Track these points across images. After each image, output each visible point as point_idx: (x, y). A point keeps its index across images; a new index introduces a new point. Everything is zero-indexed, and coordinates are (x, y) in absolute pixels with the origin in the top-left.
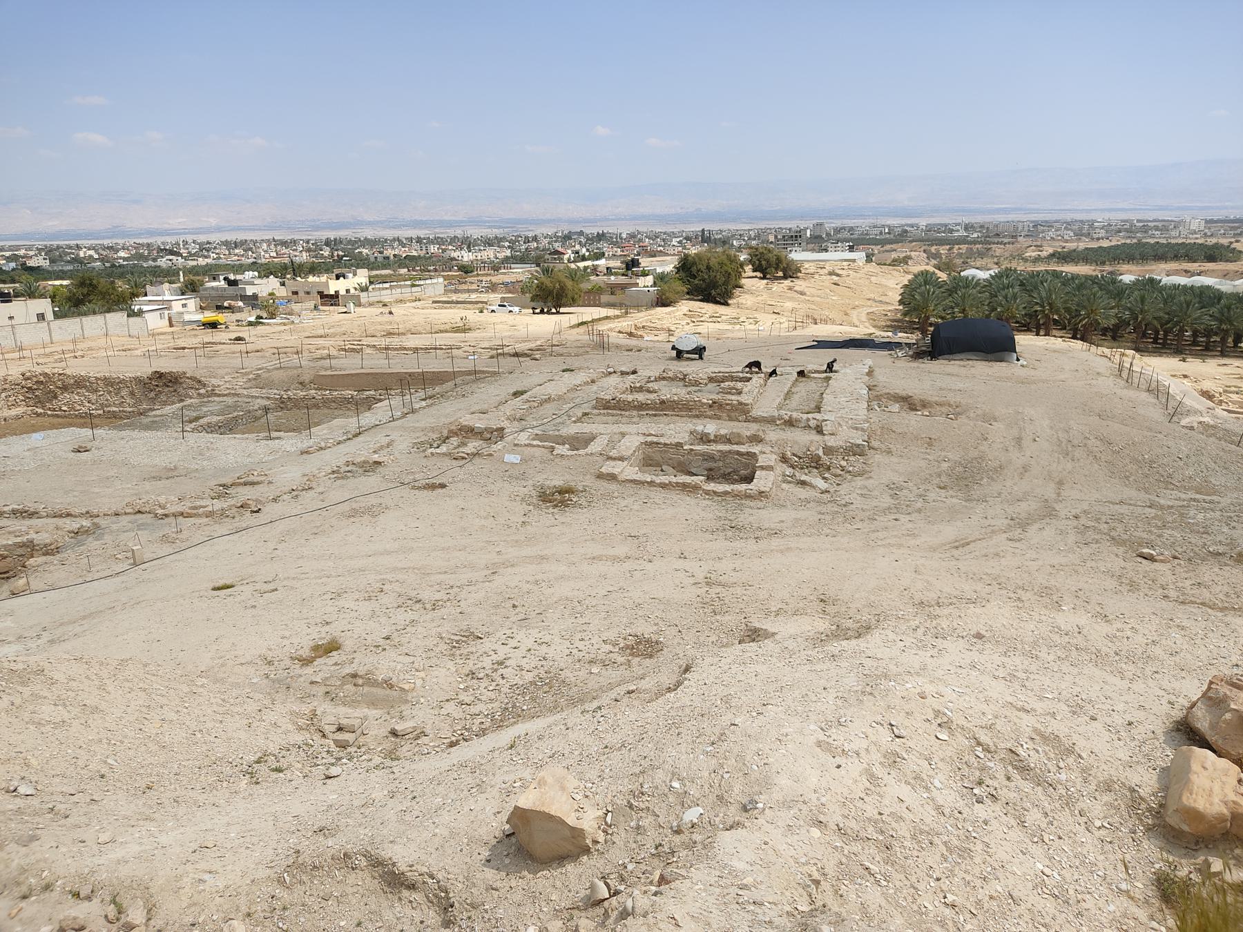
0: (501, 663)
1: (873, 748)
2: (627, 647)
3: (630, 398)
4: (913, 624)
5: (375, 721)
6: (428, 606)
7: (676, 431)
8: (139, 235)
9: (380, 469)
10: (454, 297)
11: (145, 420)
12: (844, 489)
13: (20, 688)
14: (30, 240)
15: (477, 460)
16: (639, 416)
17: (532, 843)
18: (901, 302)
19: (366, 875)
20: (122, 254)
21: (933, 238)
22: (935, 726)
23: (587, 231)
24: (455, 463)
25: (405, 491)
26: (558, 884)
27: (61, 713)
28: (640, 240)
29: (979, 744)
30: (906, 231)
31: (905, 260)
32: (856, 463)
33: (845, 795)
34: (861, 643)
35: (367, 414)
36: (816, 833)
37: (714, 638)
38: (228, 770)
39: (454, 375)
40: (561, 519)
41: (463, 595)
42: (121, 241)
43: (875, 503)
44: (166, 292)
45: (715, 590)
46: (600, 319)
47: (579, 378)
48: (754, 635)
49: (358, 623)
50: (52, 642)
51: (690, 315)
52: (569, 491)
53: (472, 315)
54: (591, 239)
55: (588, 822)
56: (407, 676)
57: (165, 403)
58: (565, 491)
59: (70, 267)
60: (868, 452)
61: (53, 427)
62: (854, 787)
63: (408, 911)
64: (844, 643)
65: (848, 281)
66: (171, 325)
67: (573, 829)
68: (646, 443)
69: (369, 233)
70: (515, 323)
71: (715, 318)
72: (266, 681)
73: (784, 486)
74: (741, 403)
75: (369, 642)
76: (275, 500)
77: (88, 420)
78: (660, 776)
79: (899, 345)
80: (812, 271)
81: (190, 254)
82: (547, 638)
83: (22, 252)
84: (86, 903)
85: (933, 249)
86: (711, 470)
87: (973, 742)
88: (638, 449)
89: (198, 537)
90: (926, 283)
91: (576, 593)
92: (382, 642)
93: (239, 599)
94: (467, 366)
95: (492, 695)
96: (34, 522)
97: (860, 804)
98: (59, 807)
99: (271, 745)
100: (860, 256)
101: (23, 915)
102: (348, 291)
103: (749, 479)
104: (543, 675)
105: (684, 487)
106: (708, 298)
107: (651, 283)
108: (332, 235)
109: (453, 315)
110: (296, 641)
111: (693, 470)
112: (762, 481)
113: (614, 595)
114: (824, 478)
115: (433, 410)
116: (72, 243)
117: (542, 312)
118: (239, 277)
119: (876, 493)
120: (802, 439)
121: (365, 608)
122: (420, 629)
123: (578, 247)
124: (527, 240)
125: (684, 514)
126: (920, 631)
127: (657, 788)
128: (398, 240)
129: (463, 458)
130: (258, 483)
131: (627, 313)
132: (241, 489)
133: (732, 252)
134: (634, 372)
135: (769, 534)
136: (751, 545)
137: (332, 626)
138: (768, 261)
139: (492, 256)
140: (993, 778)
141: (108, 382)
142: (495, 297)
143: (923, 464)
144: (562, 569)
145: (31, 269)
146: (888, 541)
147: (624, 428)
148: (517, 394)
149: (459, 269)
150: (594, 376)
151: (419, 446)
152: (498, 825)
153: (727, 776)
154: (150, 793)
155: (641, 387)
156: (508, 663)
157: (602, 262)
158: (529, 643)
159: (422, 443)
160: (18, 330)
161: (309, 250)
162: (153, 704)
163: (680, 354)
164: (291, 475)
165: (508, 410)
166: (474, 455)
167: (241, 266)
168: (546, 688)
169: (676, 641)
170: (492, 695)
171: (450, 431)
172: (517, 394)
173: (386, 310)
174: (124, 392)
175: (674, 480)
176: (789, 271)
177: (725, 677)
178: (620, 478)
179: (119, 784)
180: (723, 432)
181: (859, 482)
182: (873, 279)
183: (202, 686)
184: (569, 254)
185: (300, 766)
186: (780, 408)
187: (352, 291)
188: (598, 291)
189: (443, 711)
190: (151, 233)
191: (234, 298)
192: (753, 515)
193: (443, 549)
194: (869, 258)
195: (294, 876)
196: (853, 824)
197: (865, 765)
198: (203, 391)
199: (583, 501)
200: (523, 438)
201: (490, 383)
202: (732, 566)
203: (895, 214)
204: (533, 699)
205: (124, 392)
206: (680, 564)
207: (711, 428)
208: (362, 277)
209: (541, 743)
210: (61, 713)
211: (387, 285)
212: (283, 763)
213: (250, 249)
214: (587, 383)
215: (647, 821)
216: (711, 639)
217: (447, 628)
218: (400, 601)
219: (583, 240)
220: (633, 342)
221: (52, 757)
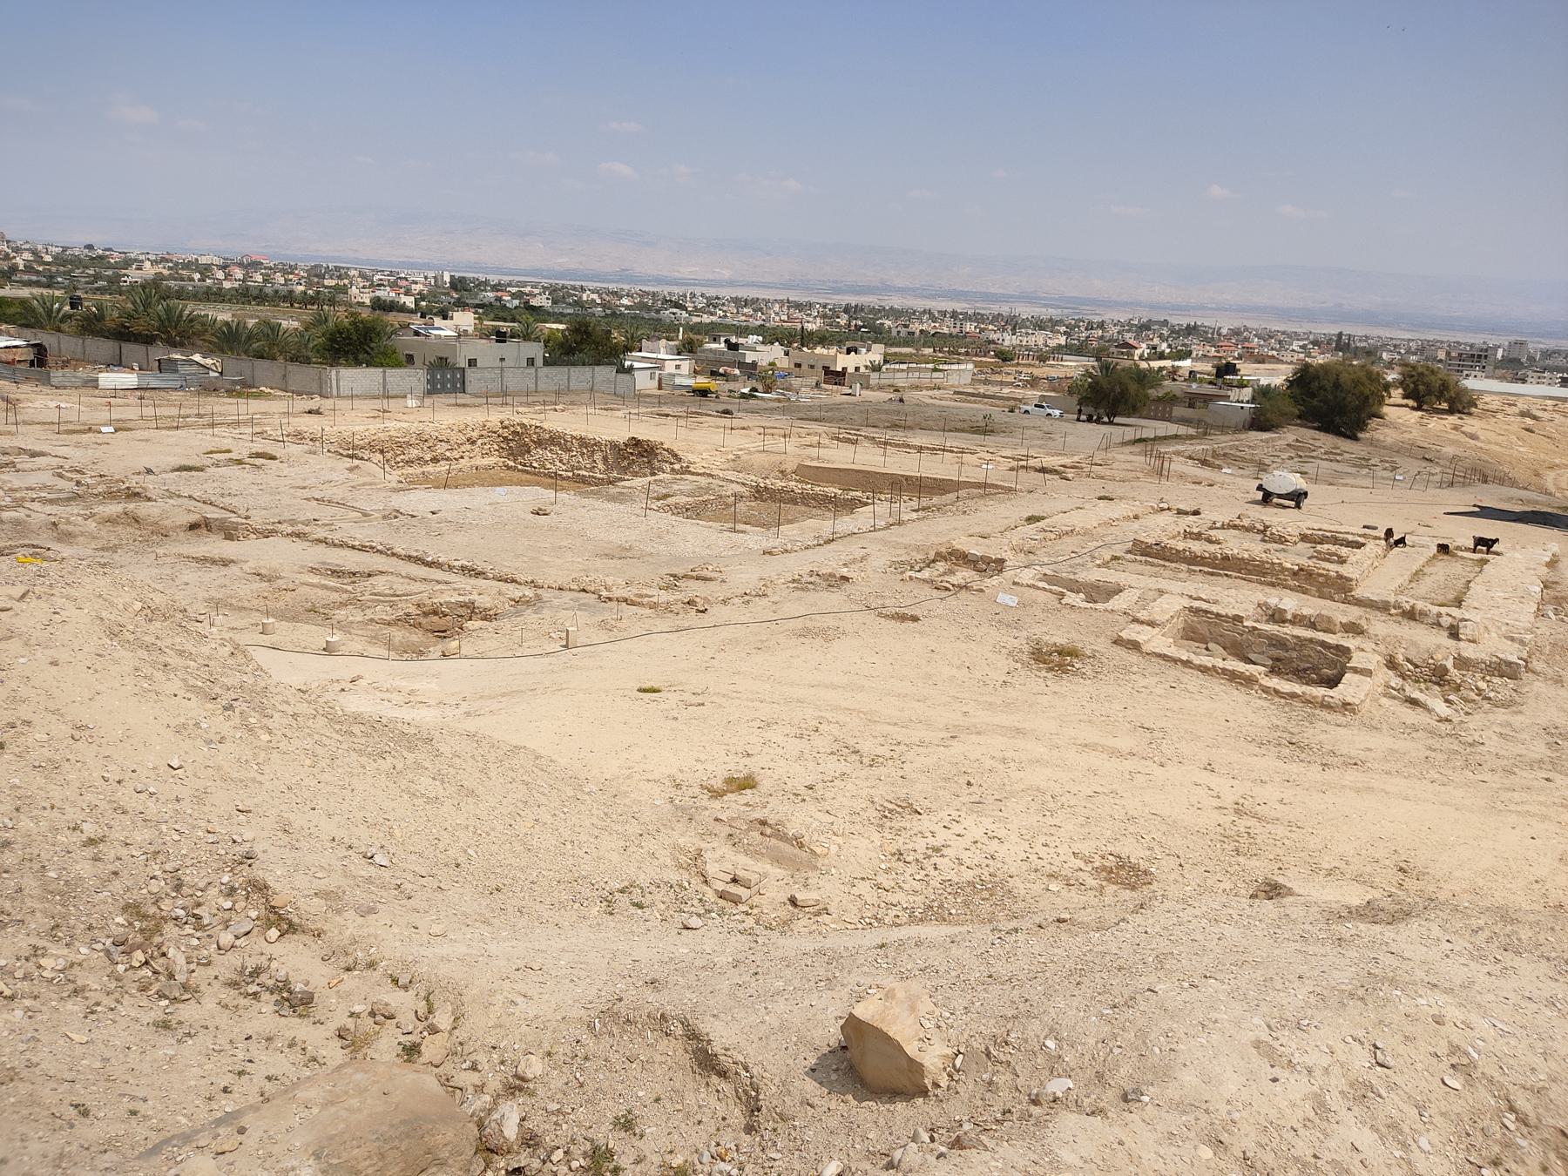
0: (937, 850)
1: (1336, 1070)
2: (1104, 868)
3: (1181, 546)
4: (1475, 923)
5: (774, 883)
6: (866, 760)
7: (1239, 600)
8: (646, 282)
9: (847, 586)
11: (612, 490)
13: (405, 753)
14: (536, 276)
15: (963, 594)
16: (1189, 571)
17: (864, 1065)
19: (679, 1045)
20: (625, 301)
22: (1446, 1062)
23: (1174, 321)
25: (870, 617)
26: (882, 1122)
27: (436, 789)
28: (1246, 339)
29: (1512, 1109)
32: (1502, 687)
33: (1271, 1118)
34: (1389, 933)
35: (846, 518)
36: (1206, 1153)
37: (1227, 885)
38: (587, 892)
40: (1054, 687)
41: (910, 756)
42: (626, 287)
43: (1520, 749)
44: (662, 351)
45: (1243, 823)
46: (1165, 438)
47: (1118, 510)
48: (1273, 890)
49: (782, 762)
50: (468, 714)
52: (1073, 653)
54: (1178, 332)
55: (933, 1059)
56: (822, 838)
57: (636, 474)
58: (1061, 652)
59: (570, 311)
60: (1524, 676)
61: (520, 483)
62: (1289, 1111)
63: (713, 1100)
64: (1362, 926)
65: (1550, 428)
66: (660, 388)
67: (911, 1060)
68: (1191, 609)
69: (896, 302)
70: (1051, 429)
72: (669, 806)
73: (1384, 701)
74: (1340, 577)
75: (789, 787)
76: (724, 602)
77: (554, 480)
78: (1035, 1027)
81: (696, 309)
82: (1002, 833)
83: (527, 289)
84: (402, 993)
86: (1278, 660)
87: (1503, 1105)
89: (637, 629)
92: (803, 791)
93: (662, 706)
95: (918, 886)
96: (480, 582)
97: (1289, 1135)
98: (407, 886)
99: (642, 876)
101: (341, 987)
102: (857, 369)
103: (1332, 682)
104: (986, 877)
105: (1232, 676)
106: (1329, 427)
108: (853, 300)
110: (710, 767)
111: (1252, 656)
112: (1350, 688)
113: (1101, 797)
114: (1447, 701)
115: (923, 525)
116: (578, 284)
117: (1090, 420)
118: (741, 341)
119: (1524, 736)
120: (1427, 642)
121: (794, 746)
122: (850, 786)
123: (1156, 341)
124: (1090, 327)
125: (1228, 715)
126: (1482, 936)
127: (1026, 1041)
128: (930, 312)
129: (947, 589)
130: (710, 579)
132: (692, 583)
134: (1196, 513)
135: (1345, 764)
136: (1314, 773)
137: (754, 759)
138: (1428, 385)
139: (1041, 342)
140: (1521, 1161)
141: (583, 442)
142: (1033, 394)
144: (1040, 750)
145: (533, 308)
146: (1526, 807)
147: (1163, 584)
148: (1032, 519)
149: (996, 356)
150: (1139, 511)
151: (898, 565)
152: (832, 1034)
153: (1116, 1051)
154: (496, 895)
155: (1200, 534)
156: (945, 851)
158: (978, 833)
159: (902, 563)
160: (508, 374)
161: (824, 316)
162: (531, 802)
163: (1267, 498)
164: (745, 576)
165: (1015, 538)
167: (747, 328)
168: (986, 894)
169: (1173, 876)
170: (918, 886)
171: (938, 554)
172: (1032, 519)
173: (898, 395)
174: (598, 456)
175: (1220, 664)
176: (1460, 404)
177: (1177, 931)
178: (1145, 648)
179: (470, 878)
181: (1501, 715)
183: (589, 794)
184: (1143, 349)
185: (663, 907)
186: (1400, 591)
187: (862, 370)
188: (1171, 399)
189: (855, 891)
190: (659, 281)
191: (732, 365)
192: (1326, 732)
195: (605, 1025)
196: (1269, 1158)
197: (1316, 1089)
198: (677, 467)
199: (1088, 670)
200: (1027, 576)
201: (1001, 501)
202: (1279, 796)
204: (966, 904)
205: (598, 456)
206: (1205, 777)
207: (1290, 602)
208: (876, 354)
209: (916, 950)
210: (436, 789)
211: (904, 367)
212: (647, 900)
213: (761, 309)
214: (1127, 518)
215: (1003, 1079)
216: (1222, 886)
217: (882, 793)
218: (835, 747)
219: (1165, 332)
220: (1205, 473)
221: (417, 832)
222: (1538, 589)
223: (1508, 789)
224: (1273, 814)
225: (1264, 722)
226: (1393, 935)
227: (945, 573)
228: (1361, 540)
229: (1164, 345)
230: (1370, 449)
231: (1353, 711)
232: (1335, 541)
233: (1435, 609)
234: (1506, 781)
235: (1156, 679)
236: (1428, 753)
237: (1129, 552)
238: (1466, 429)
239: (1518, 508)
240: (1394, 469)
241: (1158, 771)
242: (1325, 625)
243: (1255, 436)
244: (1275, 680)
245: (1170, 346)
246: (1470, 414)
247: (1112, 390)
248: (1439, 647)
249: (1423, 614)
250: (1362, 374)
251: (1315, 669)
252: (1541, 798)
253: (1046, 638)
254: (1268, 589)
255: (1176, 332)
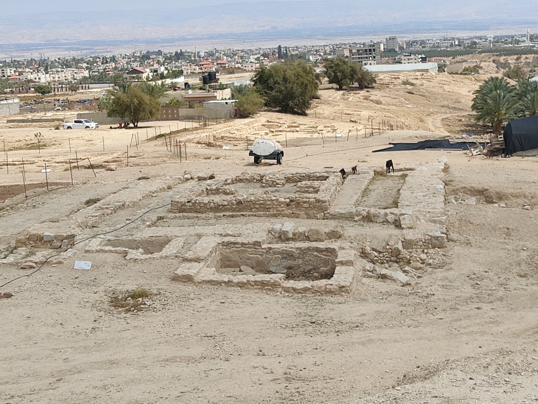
3: (206, 200)
4: (484, 362)
7: (254, 230)
10: (30, 116)
12: (425, 280)
15: (46, 269)
18: (474, 107)
21: (500, 49)
24: (22, 273)
28: (218, 58)
30: (475, 43)
31: (476, 69)
34: (428, 384)
39: (24, 188)
43: (457, 293)
46: (178, 132)
51: (268, 125)
52: (143, 294)
53: (48, 133)
54: (170, 58)
58: (134, 296)
68: (223, 244)
70: (91, 137)
71: (293, 128)
73: (365, 280)
74: (318, 201)
79: (473, 144)
80: (386, 81)
85: (502, 59)
86: (290, 268)
88: (215, 249)
90: (496, 88)
91: (146, 395)
94: (39, 178)
100: (431, 66)
103: (329, 275)
106: (286, 109)
107: (229, 96)
109: (28, 133)
111: (272, 269)
112: (342, 276)
114: (404, 271)
119: (457, 283)
120: (380, 235)
123: (156, 66)
124: (105, 61)
125: (263, 311)
126: (492, 369)
129: (31, 267)
131: (205, 125)
133: (308, 65)
134: (212, 177)
138: (342, 72)
139: (69, 77)
142: (71, 115)
143: (503, 254)
146: (471, 329)
147: (200, 230)
148: (89, 203)
150: (171, 182)
155: (217, 189)
157: (181, 80)
163: (257, 159)
165: (80, 218)
166: (43, 263)
172: (89, 203)
175: (252, 278)
176: (365, 82)
178: (197, 279)
180: (301, 230)
181: (440, 273)
182: (446, 87)
184: (147, 73)
186: (357, 204)
188: (176, 104)
193: (5, 359)
194: (441, 69)
200: (95, 244)
203: (464, 27)
206: (259, 361)
207: (289, 226)
219: (161, 59)
220: (211, 151)
222: (442, 187)
223: (456, 320)
224: (312, 374)
225: (291, 312)
226: (432, 386)
227: (27, 256)
228: (325, 174)
229: (162, 68)
230: (316, 120)
231: (347, 292)
232: (309, 177)
233: (383, 212)
234: (454, 315)
235: (210, 299)
236: (401, 308)
237: (170, 211)
238: (372, 98)
239: (416, 141)
240: (334, 130)
241: (225, 365)
242: (315, 237)
243: (239, 122)
244: (292, 282)
245: (166, 69)
246: (373, 88)
247: (132, 101)
248: (390, 236)
249: (376, 216)
250: (300, 70)
251: (315, 269)
252: (478, 321)
253: (120, 288)
254: (273, 220)
255: (169, 59)
